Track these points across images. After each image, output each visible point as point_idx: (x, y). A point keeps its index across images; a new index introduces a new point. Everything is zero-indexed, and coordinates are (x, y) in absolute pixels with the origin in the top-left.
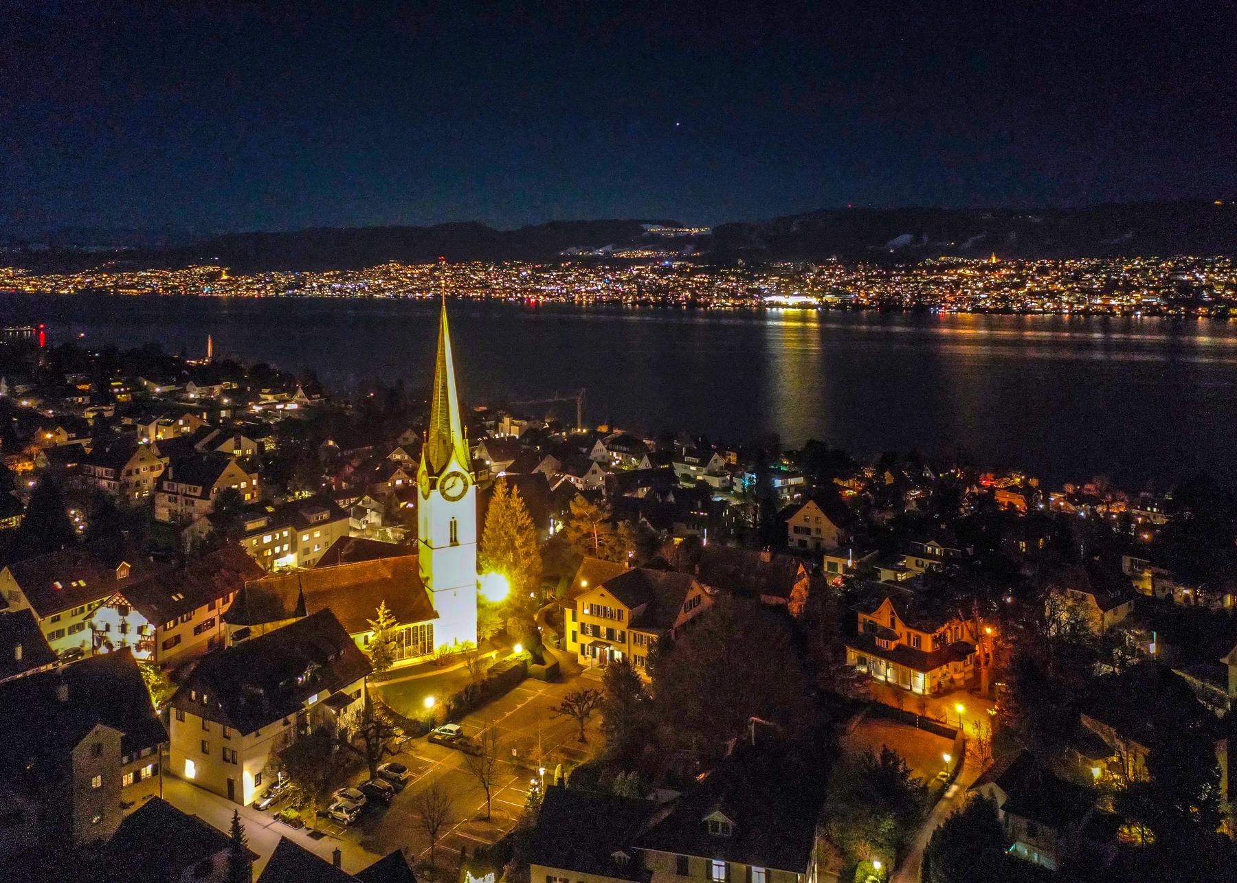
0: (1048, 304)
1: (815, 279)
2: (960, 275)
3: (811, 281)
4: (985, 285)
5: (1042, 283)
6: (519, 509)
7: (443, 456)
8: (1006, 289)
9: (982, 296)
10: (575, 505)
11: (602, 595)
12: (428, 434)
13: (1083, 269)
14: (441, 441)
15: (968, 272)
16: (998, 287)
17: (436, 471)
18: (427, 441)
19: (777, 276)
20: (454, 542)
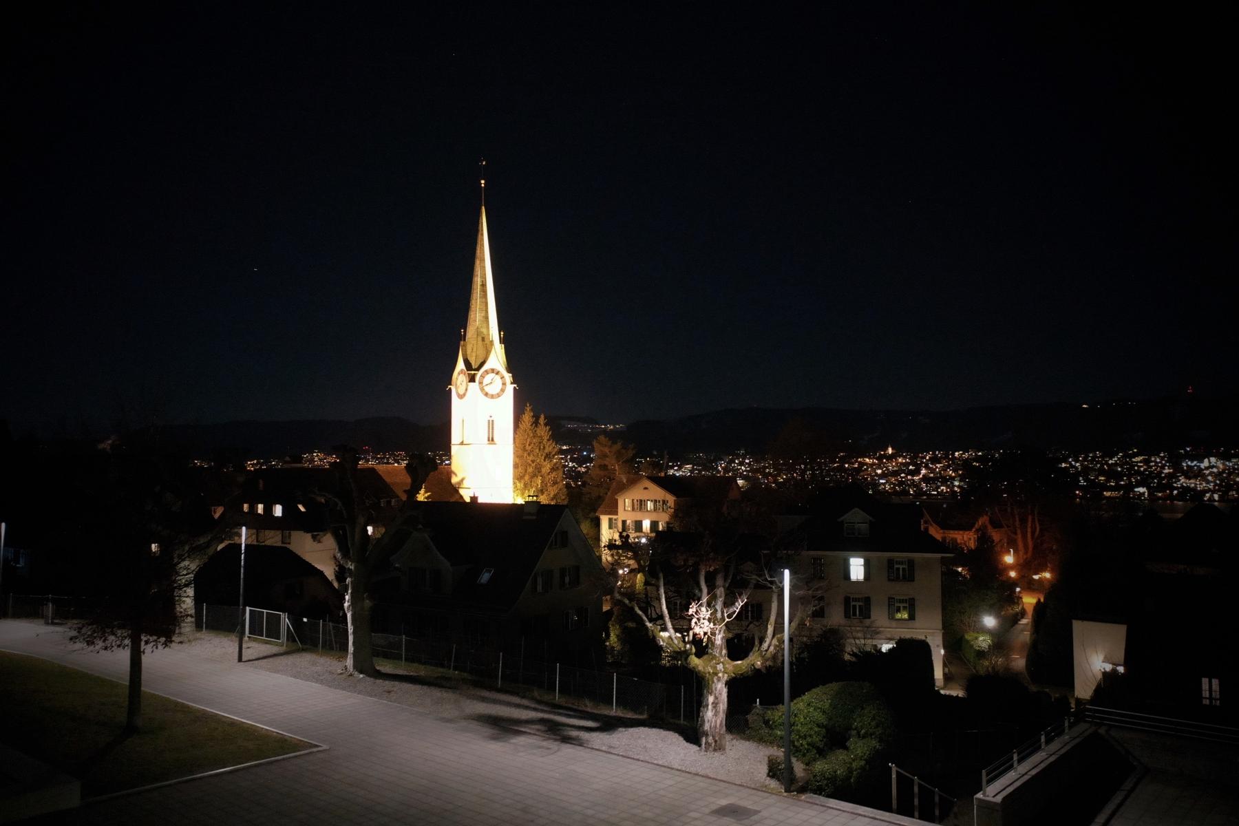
0: (942, 488)
1: (726, 466)
2: (860, 463)
3: (722, 468)
4: (883, 472)
5: (935, 469)
6: (546, 438)
7: (481, 353)
8: (903, 475)
9: (881, 481)
10: (600, 443)
11: (646, 488)
12: (465, 332)
13: (970, 459)
14: (480, 339)
15: (867, 460)
16: (895, 474)
17: (474, 366)
18: (465, 340)
19: (690, 464)
20: (491, 440)
